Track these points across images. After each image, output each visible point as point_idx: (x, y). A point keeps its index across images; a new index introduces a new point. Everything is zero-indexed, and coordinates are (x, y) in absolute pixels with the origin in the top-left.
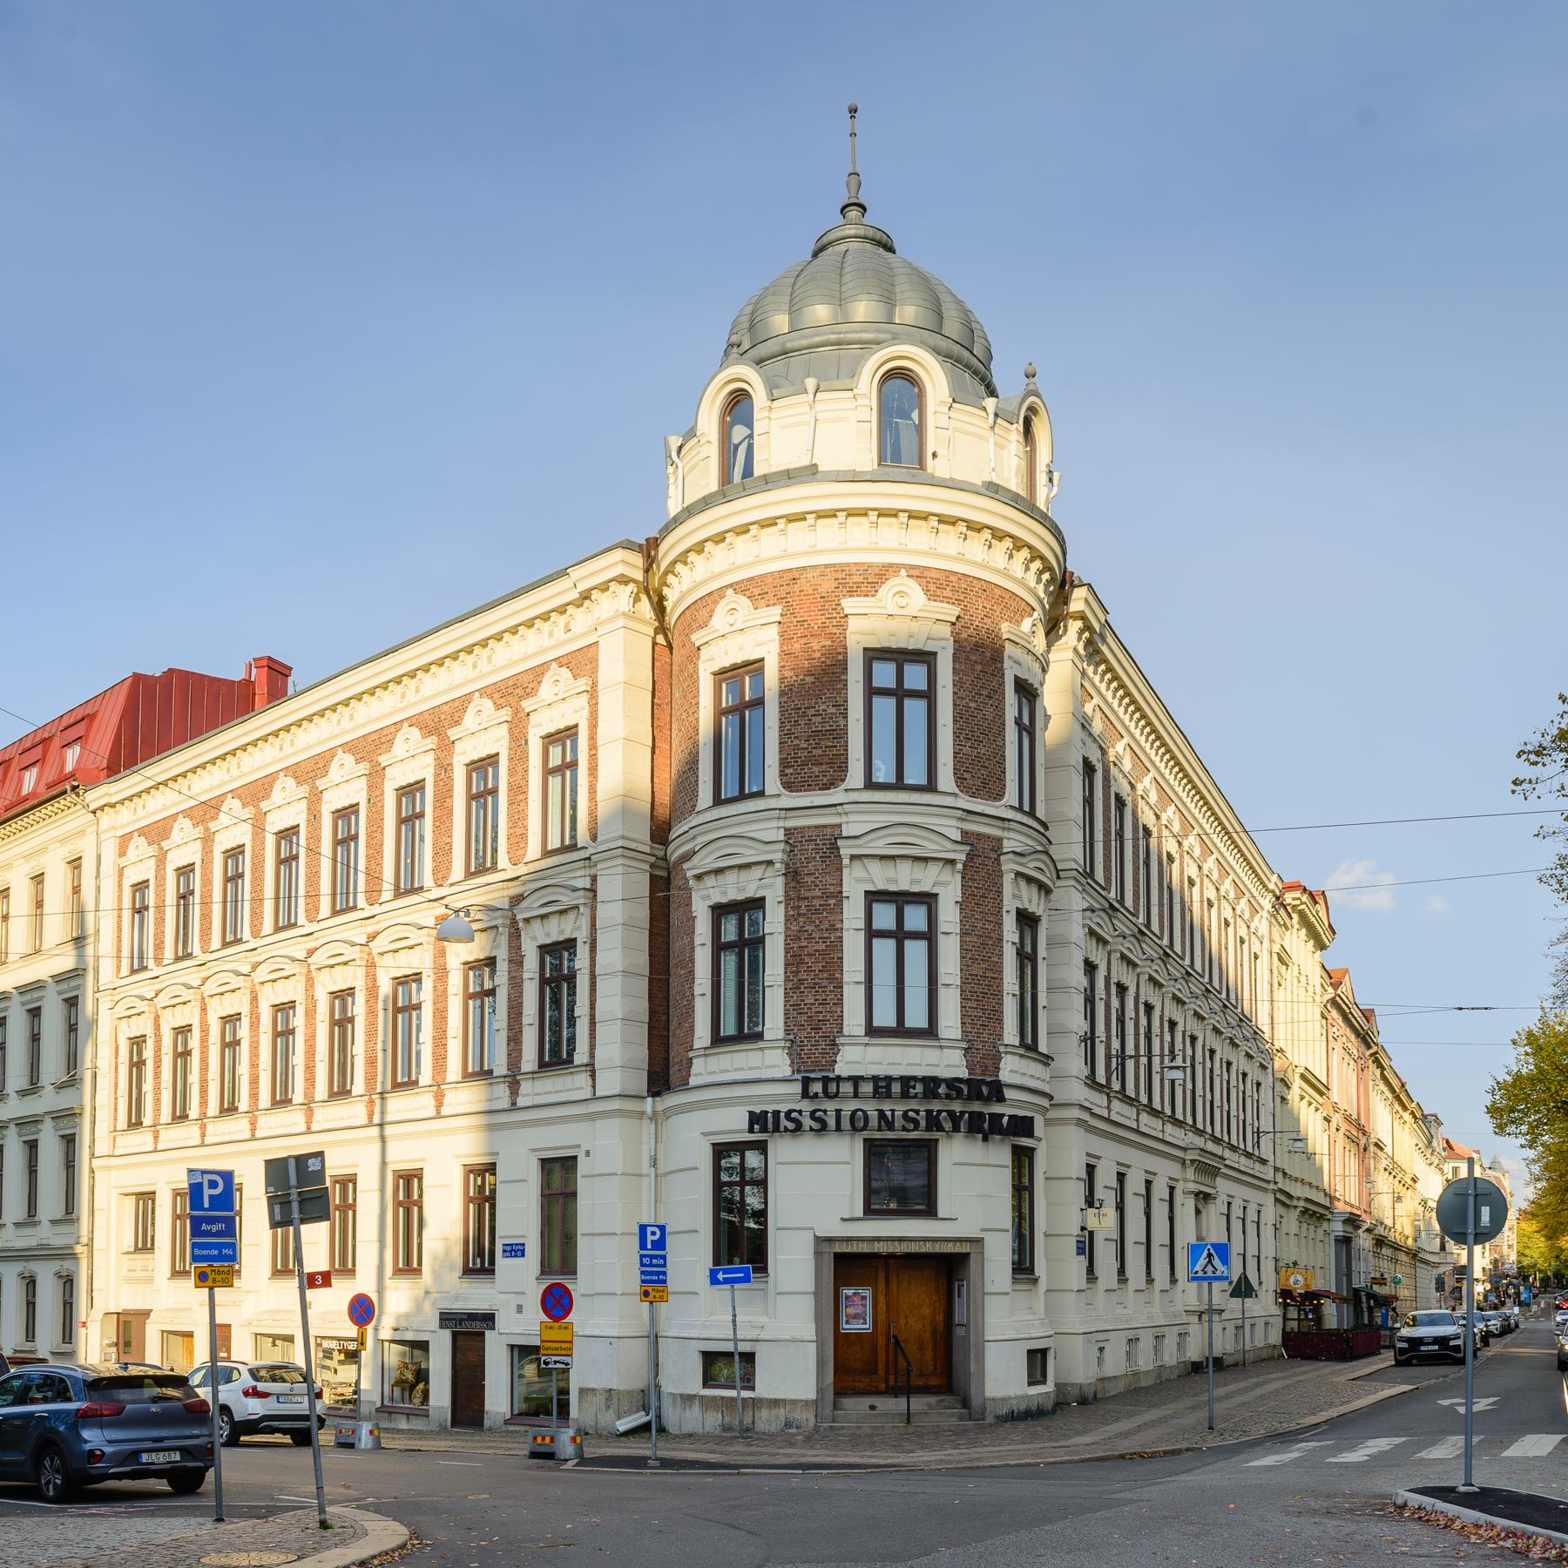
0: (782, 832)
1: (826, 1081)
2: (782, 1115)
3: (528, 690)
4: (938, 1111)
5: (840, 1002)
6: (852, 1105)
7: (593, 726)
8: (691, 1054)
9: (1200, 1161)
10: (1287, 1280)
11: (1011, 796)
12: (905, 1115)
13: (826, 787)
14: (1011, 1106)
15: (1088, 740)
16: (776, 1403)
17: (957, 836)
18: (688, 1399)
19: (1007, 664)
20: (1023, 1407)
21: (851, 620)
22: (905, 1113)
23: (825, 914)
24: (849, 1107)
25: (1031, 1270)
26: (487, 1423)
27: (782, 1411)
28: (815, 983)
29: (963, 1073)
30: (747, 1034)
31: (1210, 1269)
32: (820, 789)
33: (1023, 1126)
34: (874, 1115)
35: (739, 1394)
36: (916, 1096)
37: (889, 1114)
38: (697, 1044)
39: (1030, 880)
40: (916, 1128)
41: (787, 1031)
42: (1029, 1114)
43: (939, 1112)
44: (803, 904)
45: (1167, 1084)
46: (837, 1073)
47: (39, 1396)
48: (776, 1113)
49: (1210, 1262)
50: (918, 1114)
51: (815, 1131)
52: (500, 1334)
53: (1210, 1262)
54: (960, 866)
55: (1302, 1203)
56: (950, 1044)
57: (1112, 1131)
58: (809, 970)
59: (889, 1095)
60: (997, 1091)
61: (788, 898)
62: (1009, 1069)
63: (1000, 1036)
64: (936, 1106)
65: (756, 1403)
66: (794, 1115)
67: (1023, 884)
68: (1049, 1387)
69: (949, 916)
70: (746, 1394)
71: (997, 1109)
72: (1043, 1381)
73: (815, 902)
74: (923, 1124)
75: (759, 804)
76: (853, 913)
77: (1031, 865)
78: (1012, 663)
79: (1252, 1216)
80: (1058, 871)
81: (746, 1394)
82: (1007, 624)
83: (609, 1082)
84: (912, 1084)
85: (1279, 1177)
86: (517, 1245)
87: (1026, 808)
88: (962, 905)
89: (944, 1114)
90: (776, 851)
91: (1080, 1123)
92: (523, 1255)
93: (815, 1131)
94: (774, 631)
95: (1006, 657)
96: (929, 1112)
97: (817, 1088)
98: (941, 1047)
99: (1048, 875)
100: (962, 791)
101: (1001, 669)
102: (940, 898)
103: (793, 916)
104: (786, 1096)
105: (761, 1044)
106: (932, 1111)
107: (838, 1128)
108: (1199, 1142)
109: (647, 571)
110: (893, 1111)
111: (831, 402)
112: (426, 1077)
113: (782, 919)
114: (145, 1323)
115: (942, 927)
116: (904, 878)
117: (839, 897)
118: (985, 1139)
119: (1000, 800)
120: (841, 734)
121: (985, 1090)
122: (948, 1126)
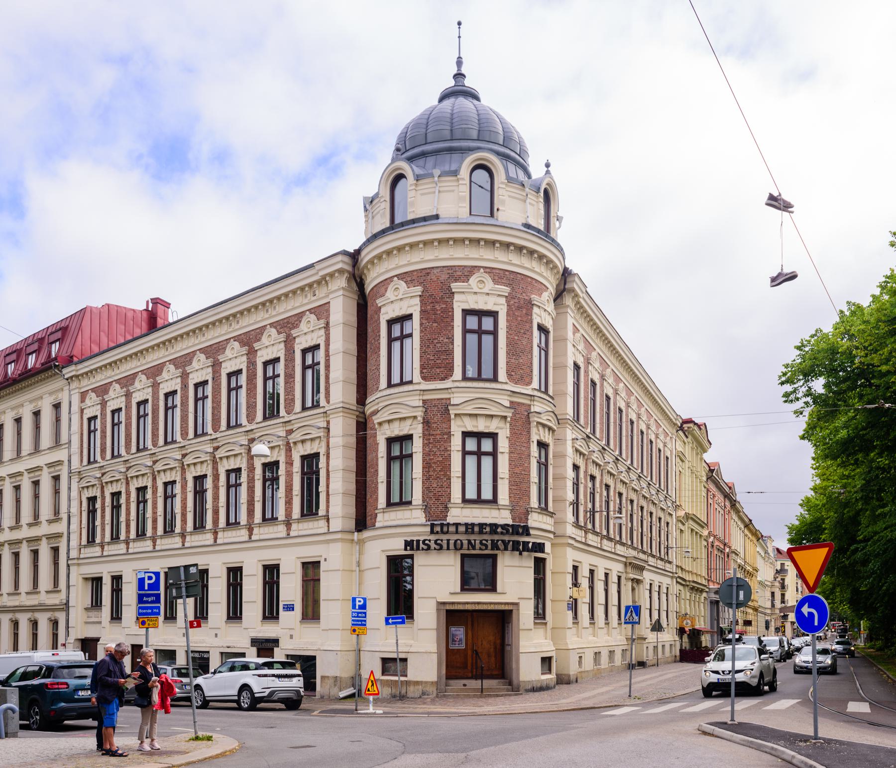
0: (421, 401)
1: (442, 525)
3: (295, 325)
13: (443, 379)
15: (577, 353)
16: (417, 683)
19: (534, 316)
20: (539, 685)
24: (453, 537)
27: (421, 687)
30: (404, 503)
31: (631, 618)
32: (440, 380)
33: (540, 547)
34: (465, 542)
36: (486, 533)
37: (473, 542)
40: (486, 549)
41: (424, 501)
42: (542, 541)
43: (498, 541)
46: (448, 521)
48: (418, 541)
49: (631, 615)
53: (631, 615)
58: (434, 471)
59: (473, 532)
60: (526, 531)
64: (496, 537)
65: (408, 683)
70: (403, 679)
71: (526, 539)
74: (490, 547)
76: (456, 442)
77: (545, 418)
84: (484, 527)
87: (543, 389)
88: (510, 439)
89: (500, 542)
92: (293, 610)
96: (492, 541)
97: (438, 529)
98: (499, 509)
104: (422, 533)
105: (411, 507)
107: (448, 549)
110: (475, 540)
115: (500, 449)
116: (481, 426)
117: (449, 434)
118: (521, 554)
120: (451, 353)
122: (502, 547)
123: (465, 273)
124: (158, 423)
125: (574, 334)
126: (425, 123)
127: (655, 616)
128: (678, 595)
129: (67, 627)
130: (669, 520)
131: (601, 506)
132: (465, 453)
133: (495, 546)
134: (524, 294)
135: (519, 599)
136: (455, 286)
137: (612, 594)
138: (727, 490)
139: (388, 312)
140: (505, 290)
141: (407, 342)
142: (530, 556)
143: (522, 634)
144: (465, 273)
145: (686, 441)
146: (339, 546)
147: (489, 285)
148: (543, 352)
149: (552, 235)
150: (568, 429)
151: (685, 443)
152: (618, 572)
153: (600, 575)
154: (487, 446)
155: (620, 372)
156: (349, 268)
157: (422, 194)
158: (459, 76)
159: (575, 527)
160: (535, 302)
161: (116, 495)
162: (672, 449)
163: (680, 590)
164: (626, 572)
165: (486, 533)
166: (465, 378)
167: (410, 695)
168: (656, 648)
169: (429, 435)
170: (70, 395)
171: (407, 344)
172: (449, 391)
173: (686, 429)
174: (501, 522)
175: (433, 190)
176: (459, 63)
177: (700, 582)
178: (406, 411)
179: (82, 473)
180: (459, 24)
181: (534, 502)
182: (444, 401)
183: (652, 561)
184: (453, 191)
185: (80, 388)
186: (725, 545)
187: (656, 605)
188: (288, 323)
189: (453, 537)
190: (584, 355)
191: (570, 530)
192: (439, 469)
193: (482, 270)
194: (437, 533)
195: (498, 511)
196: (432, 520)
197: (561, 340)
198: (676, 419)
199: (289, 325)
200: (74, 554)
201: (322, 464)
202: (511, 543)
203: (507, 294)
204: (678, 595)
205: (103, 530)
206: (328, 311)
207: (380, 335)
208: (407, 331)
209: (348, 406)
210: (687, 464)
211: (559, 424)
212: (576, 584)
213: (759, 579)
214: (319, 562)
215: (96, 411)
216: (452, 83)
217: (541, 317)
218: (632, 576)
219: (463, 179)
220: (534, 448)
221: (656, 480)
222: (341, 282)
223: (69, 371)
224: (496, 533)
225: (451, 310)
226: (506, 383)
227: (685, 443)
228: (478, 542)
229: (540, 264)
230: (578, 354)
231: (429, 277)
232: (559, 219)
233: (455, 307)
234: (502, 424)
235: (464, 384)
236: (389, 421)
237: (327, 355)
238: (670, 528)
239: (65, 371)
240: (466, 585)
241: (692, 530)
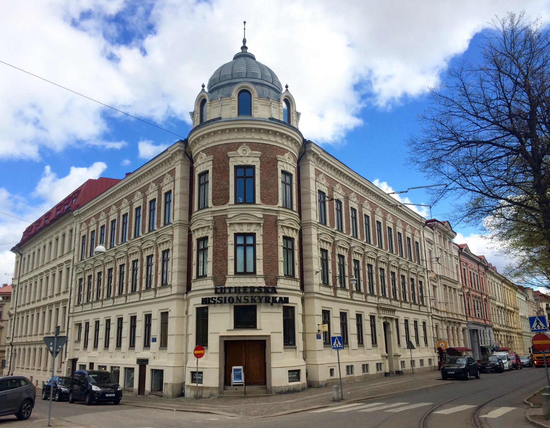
0: (212, 217)
1: (221, 289)
5: (227, 265)
6: (230, 295)
7: (174, 190)
11: (280, 203)
13: (224, 204)
14: (279, 294)
16: (208, 388)
17: (261, 216)
19: (279, 166)
20: (287, 389)
24: (228, 296)
26: (145, 393)
29: (263, 285)
31: (337, 345)
34: (235, 298)
37: (239, 298)
38: (193, 279)
40: (248, 302)
41: (213, 274)
44: (218, 237)
45: (463, 270)
49: (337, 343)
53: (337, 343)
54: (262, 225)
56: (260, 276)
58: (219, 256)
59: (239, 292)
61: (214, 235)
65: (202, 388)
66: (220, 299)
67: (285, 229)
70: (199, 385)
71: (275, 295)
74: (250, 301)
75: (207, 210)
76: (231, 239)
77: (287, 223)
81: (199, 385)
83: (175, 290)
88: (263, 236)
94: (211, 163)
97: (219, 291)
98: (257, 278)
104: (211, 294)
105: (206, 278)
107: (225, 302)
109: (185, 148)
110: (241, 297)
111: (226, 101)
113: (212, 242)
115: (257, 242)
117: (227, 235)
118: (272, 304)
120: (227, 189)
123: (235, 146)
126: (231, 73)
129: (66, 353)
130: (422, 279)
132: (236, 246)
133: (253, 300)
134: (271, 155)
135: (271, 333)
136: (230, 154)
137: (365, 328)
138: (479, 260)
139: (198, 170)
140: (259, 153)
142: (279, 306)
143: (273, 355)
144: (235, 146)
146: (175, 302)
147: (249, 151)
149: (293, 123)
154: (250, 241)
156: (183, 149)
157: (213, 108)
158: (244, 48)
160: (279, 159)
162: (421, 237)
164: (379, 313)
166: (236, 203)
167: (204, 396)
170: (76, 225)
172: (227, 210)
175: (218, 105)
176: (244, 41)
177: (456, 318)
178: (203, 223)
180: (245, 22)
182: (224, 216)
184: (229, 105)
185: (80, 221)
186: (482, 294)
192: (221, 255)
193: (244, 144)
194: (219, 293)
195: (256, 279)
200: (71, 311)
209: (182, 222)
213: (520, 314)
214: (168, 312)
216: (241, 51)
218: (383, 316)
219: (234, 98)
220: (281, 241)
222: (180, 157)
223: (75, 213)
224: (254, 292)
226: (260, 204)
228: (242, 298)
229: (282, 138)
231: (217, 150)
232: (298, 115)
233: (230, 164)
234: (258, 228)
235: (234, 206)
239: (74, 213)
240: (239, 324)
241: (445, 286)
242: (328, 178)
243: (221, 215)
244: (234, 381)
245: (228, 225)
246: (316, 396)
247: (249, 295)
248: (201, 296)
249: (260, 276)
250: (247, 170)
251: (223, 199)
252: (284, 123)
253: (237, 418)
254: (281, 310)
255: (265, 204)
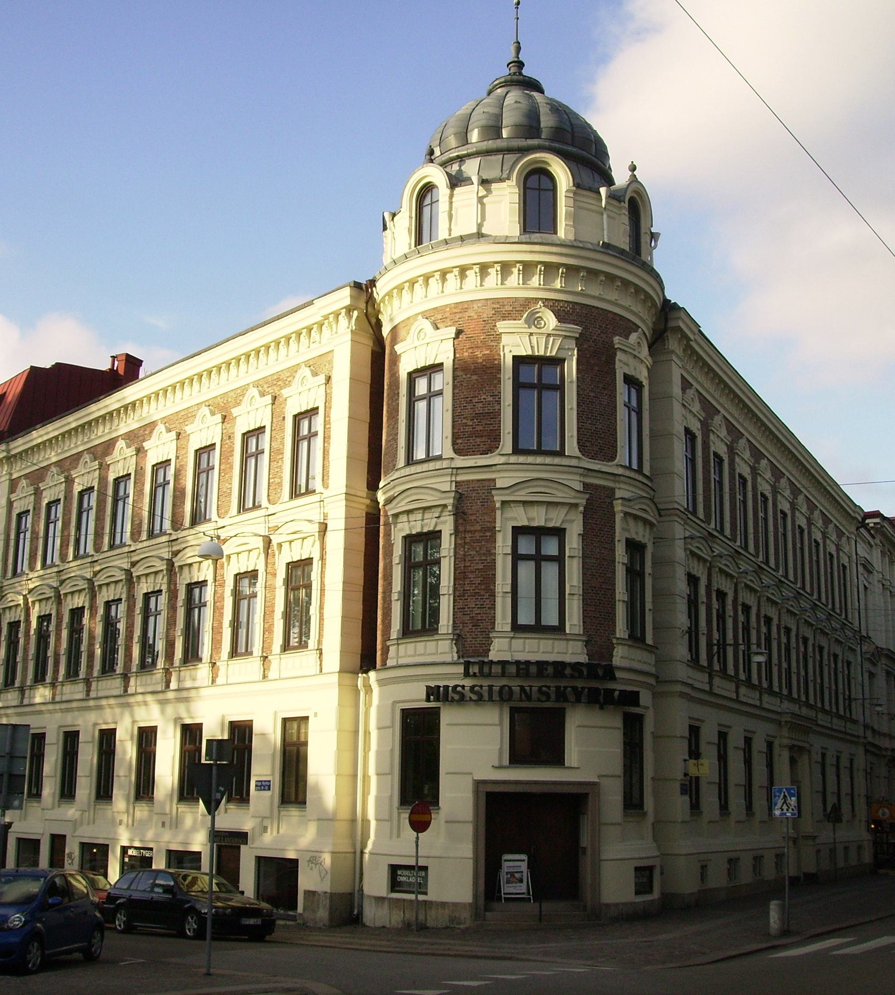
1: (482, 664)
2: (450, 688)
3: (287, 382)
4: (564, 687)
6: (503, 682)
8: (388, 643)
9: (792, 723)
10: (877, 812)
11: (622, 456)
12: (540, 690)
13: (485, 453)
15: (689, 416)
16: (443, 905)
17: (580, 487)
18: (380, 900)
19: (618, 365)
21: (504, 337)
22: (540, 689)
23: (483, 543)
24: (498, 683)
25: (640, 805)
28: (476, 593)
29: (583, 659)
30: (429, 627)
32: (481, 454)
33: (632, 698)
34: (516, 690)
35: (417, 897)
36: (548, 676)
37: (527, 689)
39: (636, 517)
42: (636, 689)
43: (566, 688)
44: (468, 535)
46: (490, 658)
47: (189, 865)
48: (446, 687)
50: (549, 689)
51: (473, 701)
52: (250, 848)
54: (581, 509)
55: (889, 753)
56: (574, 637)
57: (710, 699)
58: (471, 583)
60: (610, 672)
62: (620, 655)
63: (614, 632)
64: (563, 683)
67: (631, 522)
68: (656, 895)
69: (573, 543)
70: (421, 897)
71: (611, 685)
72: (650, 891)
73: (477, 534)
74: (553, 696)
76: (503, 544)
77: (637, 507)
78: (621, 365)
79: (844, 762)
80: (658, 510)
81: (421, 897)
82: (617, 337)
84: (545, 667)
85: (869, 734)
86: (265, 781)
87: (635, 466)
88: (584, 536)
89: (569, 689)
90: (449, 498)
91: (682, 695)
92: (269, 789)
93: (473, 701)
95: (617, 362)
96: (558, 688)
97: (475, 669)
99: (651, 514)
100: (583, 455)
101: (614, 369)
102: (567, 530)
103: (461, 544)
105: (436, 637)
106: (560, 687)
107: (491, 699)
108: (795, 708)
112: (257, 649)
114: (8, 832)
116: (538, 518)
117: (492, 530)
119: (613, 461)
120: (495, 415)
121: (600, 672)
122: (572, 698)
124: (104, 519)
125: (684, 390)
127: (831, 800)
128: (869, 771)
130: (851, 659)
131: (735, 637)
132: (517, 558)
134: (603, 336)
141: (437, 402)
145: (873, 543)
148: (633, 414)
150: (676, 524)
151: (871, 546)
152: (768, 735)
153: (735, 740)
154: (550, 547)
155: (761, 444)
159: (691, 666)
161: (76, 613)
163: (872, 763)
165: (548, 676)
168: (833, 851)
169: (465, 531)
171: (436, 405)
172: (494, 468)
173: (871, 525)
174: (568, 659)
179: (4, 588)
181: (621, 629)
182: (487, 483)
183: (822, 719)
187: (831, 787)
188: (278, 379)
189: (498, 683)
190: (702, 419)
191: (683, 672)
192: (478, 580)
194: (475, 675)
196: (468, 657)
197: (660, 398)
198: (854, 512)
199: (279, 383)
201: (315, 576)
202: (586, 690)
203: (577, 336)
204: (869, 771)
205: (25, 669)
206: (330, 362)
207: (398, 393)
208: (437, 386)
210: (876, 577)
211: (660, 515)
212: (695, 753)
215: (28, 503)
217: (628, 365)
221: (827, 598)
225: (496, 357)
227: (871, 546)
230: (692, 417)
231: (467, 314)
232: (654, 236)
235: (513, 459)
236: (409, 512)
237: (327, 423)
238: (852, 671)
242: (703, 400)
243: (478, 480)
244: (508, 889)
245: (498, 505)
246: (246, 987)
247: (552, 684)
248: (426, 680)
249: (574, 637)
250: (547, 370)
251: (484, 439)
252: (622, 252)
253: (578, 969)
254: (618, 722)
255: (588, 456)
